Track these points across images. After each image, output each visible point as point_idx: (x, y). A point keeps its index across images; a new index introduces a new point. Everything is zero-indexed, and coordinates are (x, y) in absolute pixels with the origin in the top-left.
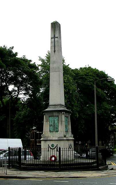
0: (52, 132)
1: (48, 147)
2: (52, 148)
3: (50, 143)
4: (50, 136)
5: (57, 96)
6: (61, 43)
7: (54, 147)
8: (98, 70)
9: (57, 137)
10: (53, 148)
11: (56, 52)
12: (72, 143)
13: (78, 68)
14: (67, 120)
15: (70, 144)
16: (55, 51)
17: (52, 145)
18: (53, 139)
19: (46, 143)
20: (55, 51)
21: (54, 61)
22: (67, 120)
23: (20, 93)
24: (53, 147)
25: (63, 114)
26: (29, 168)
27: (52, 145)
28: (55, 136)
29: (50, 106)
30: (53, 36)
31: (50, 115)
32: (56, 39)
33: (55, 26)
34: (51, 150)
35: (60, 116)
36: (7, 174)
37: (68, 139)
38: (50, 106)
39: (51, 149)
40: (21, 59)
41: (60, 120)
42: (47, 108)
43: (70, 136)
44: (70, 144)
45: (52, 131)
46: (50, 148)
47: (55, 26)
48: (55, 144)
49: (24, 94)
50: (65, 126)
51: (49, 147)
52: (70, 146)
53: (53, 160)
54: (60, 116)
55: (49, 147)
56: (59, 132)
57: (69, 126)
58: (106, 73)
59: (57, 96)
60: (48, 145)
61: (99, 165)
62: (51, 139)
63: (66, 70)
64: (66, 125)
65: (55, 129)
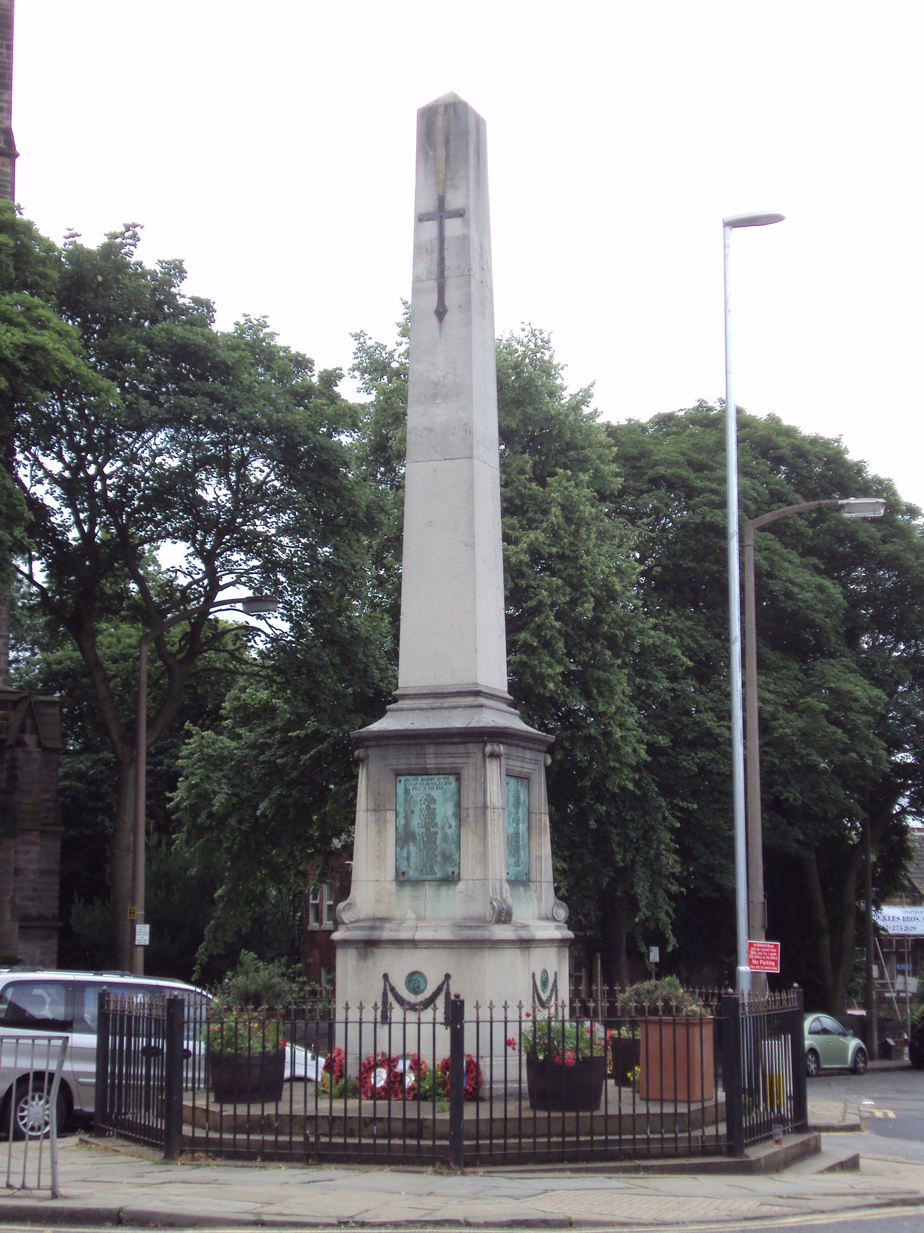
0: (416, 883)
1: (385, 995)
2: (412, 996)
3: (398, 966)
4: (398, 913)
5: (454, 629)
6: (485, 253)
7: (427, 994)
8: (790, 432)
9: (455, 918)
10: (421, 998)
11: (447, 318)
12: (557, 965)
13: (644, 417)
14: (523, 796)
15: (545, 972)
16: (441, 313)
17: (415, 980)
18: (419, 935)
19: (370, 962)
20: (441, 313)
21: (437, 384)
22: (523, 796)
23: (221, 596)
24: (416, 991)
25: (494, 756)
26: (345, 1146)
27: (415, 980)
28: (435, 913)
29: (404, 697)
30: (430, 205)
31: (402, 764)
32: (453, 227)
33: (448, 138)
34: (412, 1016)
35: (468, 774)
36: (55, 1196)
37: (524, 934)
38: (404, 697)
39: (413, 1007)
40: (235, 342)
41: (469, 799)
42: (380, 713)
43: (541, 914)
44: (545, 972)
45: (413, 874)
46: (401, 1001)
47: (448, 138)
48: (434, 969)
49: (246, 601)
50: (509, 844)
51: (389, 989)
52: (545, 983)
53: (379, 1085)
54: (471, 770)
55: (389, 989)
56: (461, 886)
57: (533, 845)
58: (852, 456)
59: (454, 629)
60: (386, 976)
61: (745, 1129)
62: (404, 935)
63: (537, 429)
64: (517, 834)
65: (430, 864)
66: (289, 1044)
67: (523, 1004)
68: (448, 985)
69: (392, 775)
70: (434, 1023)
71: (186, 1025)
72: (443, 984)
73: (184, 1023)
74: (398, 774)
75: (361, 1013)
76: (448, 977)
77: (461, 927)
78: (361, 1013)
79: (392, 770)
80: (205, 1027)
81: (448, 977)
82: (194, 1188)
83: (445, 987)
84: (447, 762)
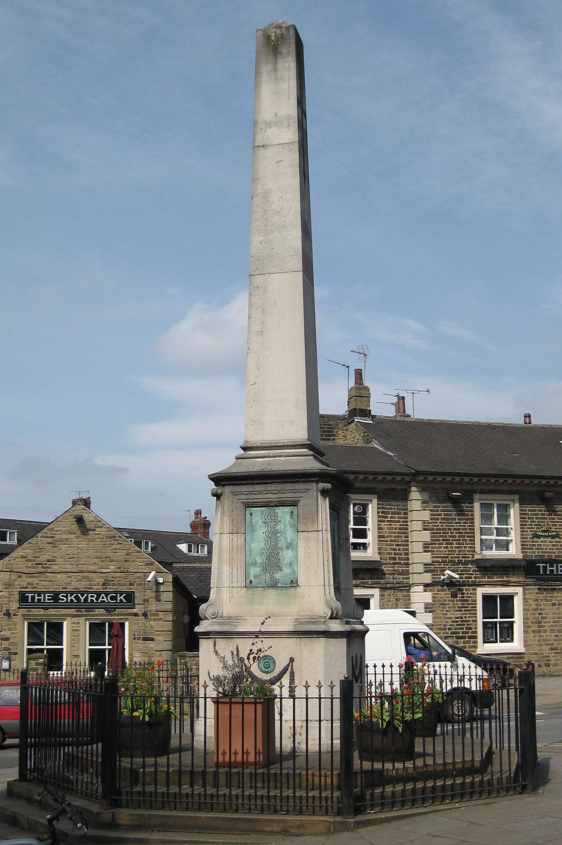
7: (276, 673)
66: (439, 725)
67: (322, 684)
68: (292, 666)
69: (243, 507)
70: (332, 699)
71: (277, 700)
72: (288, 665)
73: (275, 697)
74: (249, 505)
75: (332, 692)
76: (292, 660)
77: (301, 623)
78: (332, 692)
79: (242, 503)
80: (493, 713)
81: (292, 660)
82: (235, 836)
83: (290, 668)
84: (288, 496)
